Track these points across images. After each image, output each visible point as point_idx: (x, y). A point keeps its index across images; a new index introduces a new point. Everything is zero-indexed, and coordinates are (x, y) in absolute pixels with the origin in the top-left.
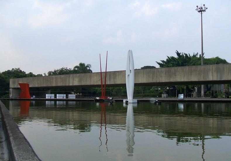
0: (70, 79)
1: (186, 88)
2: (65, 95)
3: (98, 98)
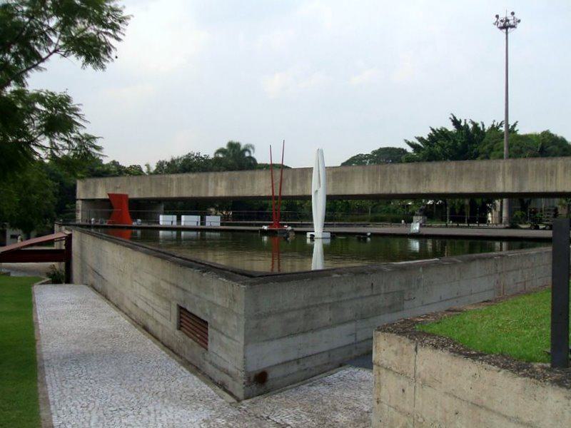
1: (470, 203)
2: (175, 217)
3: (265, 228)
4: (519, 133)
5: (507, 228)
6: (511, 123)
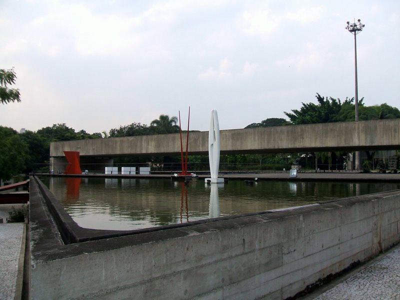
0: (143, 143)
3: (176, 175)
4: (364, 105)
5: (361, 173)
6: (359, 99)
